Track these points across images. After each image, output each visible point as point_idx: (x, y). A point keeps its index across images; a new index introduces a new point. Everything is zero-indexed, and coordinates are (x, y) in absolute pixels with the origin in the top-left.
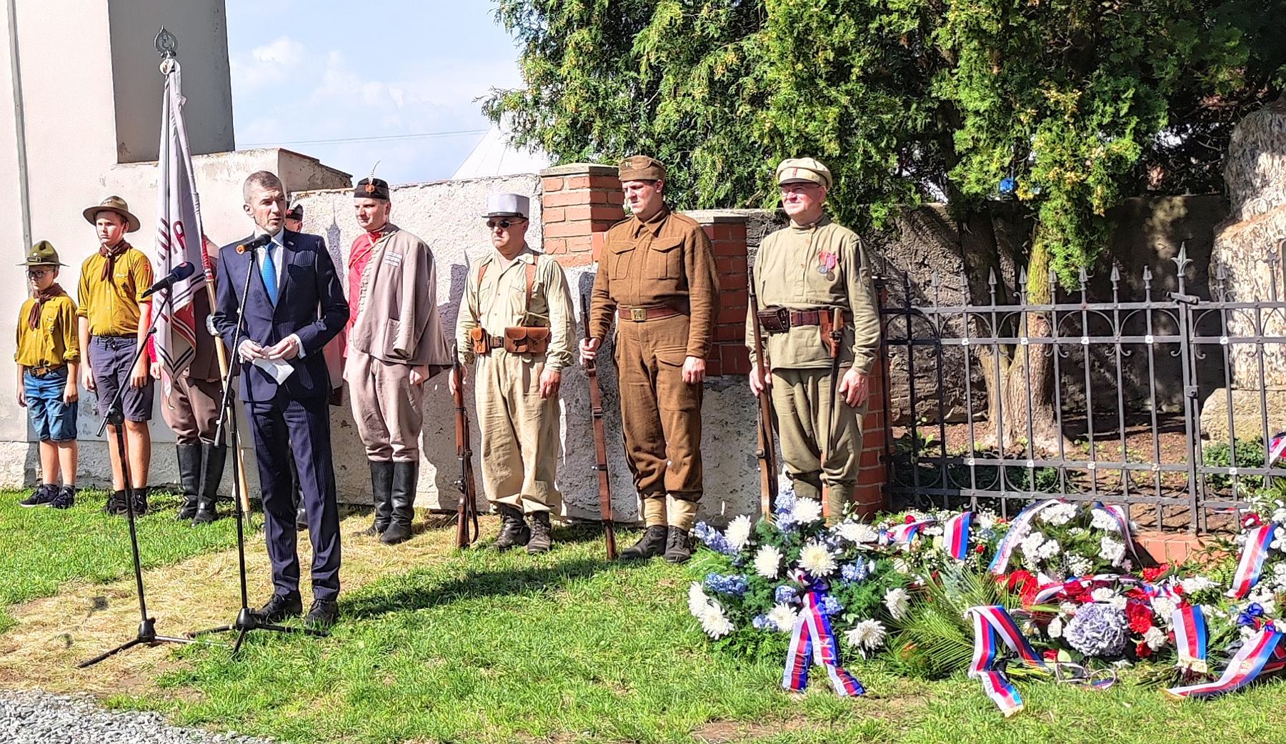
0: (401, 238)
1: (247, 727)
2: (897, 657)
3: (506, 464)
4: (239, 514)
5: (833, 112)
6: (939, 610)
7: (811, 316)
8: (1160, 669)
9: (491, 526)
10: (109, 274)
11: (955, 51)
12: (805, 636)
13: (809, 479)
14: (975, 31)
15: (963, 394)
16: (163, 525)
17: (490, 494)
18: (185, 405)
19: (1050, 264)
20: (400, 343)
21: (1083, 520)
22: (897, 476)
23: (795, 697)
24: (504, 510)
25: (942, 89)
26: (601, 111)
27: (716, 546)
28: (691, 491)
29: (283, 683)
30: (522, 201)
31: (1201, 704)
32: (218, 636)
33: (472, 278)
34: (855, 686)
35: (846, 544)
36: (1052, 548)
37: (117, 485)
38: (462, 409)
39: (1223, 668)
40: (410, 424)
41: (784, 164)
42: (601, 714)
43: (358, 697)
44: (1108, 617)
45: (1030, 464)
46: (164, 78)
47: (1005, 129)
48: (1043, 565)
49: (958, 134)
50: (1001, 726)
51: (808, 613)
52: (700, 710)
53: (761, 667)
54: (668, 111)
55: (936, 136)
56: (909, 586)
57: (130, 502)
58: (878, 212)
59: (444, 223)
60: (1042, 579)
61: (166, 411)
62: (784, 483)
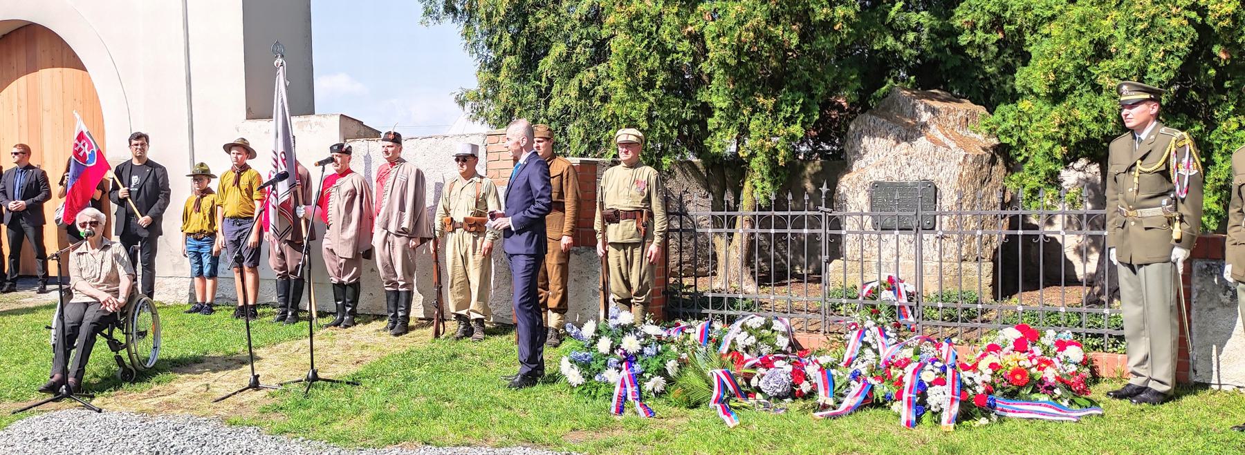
0: (407, 166)
1: (311, 435)
2: (671, 397)
3: (460, 293)
4: (310, 319)
5: (646, 105)
6: (696, 372)
7: (633, 214)
8: (810, 403)
9: (452, 326)
10: (237, 182)
11: (711, 76)
12: (623, 385)
13: (626, 302)
14: (723, 63)
15: (705, 261)
16: (265, 325)
17: (453, 310)
18: (282, 255)
19: (756, 189)
20: (405, 224)
21: (768, 326)
22: (672, 304)
23: (618, 418)
24: (459, 317)
25: (703, 96)
26: (520, 103)
27: (577, 337)
28: (561, 309)
29: (333, 411)
30: (475, 147)
31: (830, 421)
32: (296, 385)
33: (446, 190)
34: (650, 412)
35: (646, 336)
36: (753, 340)
37: (241, 303)
38: (437, 261)
39: (840, 403)
40: (409, 269)
41: (620, 132)
42: (512, 426)
43: (376, 418)
44: (783, 376)
45: (741, 296)
46: (276, 69)
47: (735, 119)
48: (747, 349)
49: (710, 120)
50: (728, 433)
51: (625, 373)
52: (567, 424)
53: (599, 402)
54: (556, 103)
55: (698, 122)
56: (679, 360)
57: (247, 312)
58: (666, 161)
59: (431, 158)
60: (746, 356)
61: (270, 263)
62: (612, 305)
